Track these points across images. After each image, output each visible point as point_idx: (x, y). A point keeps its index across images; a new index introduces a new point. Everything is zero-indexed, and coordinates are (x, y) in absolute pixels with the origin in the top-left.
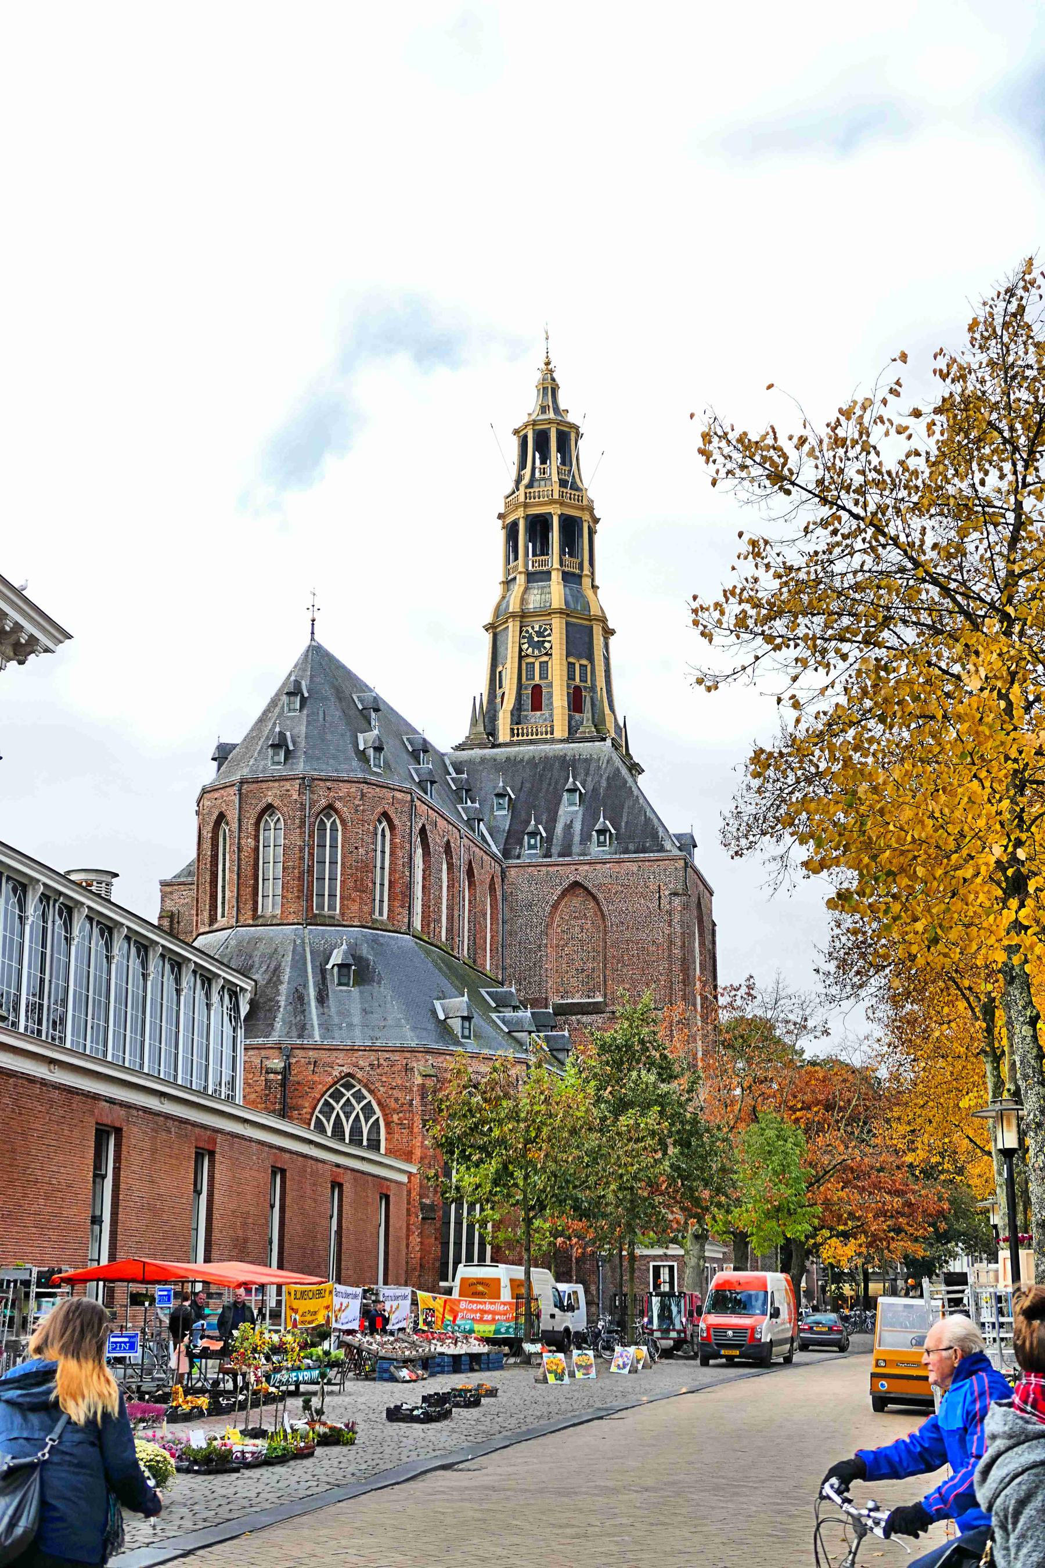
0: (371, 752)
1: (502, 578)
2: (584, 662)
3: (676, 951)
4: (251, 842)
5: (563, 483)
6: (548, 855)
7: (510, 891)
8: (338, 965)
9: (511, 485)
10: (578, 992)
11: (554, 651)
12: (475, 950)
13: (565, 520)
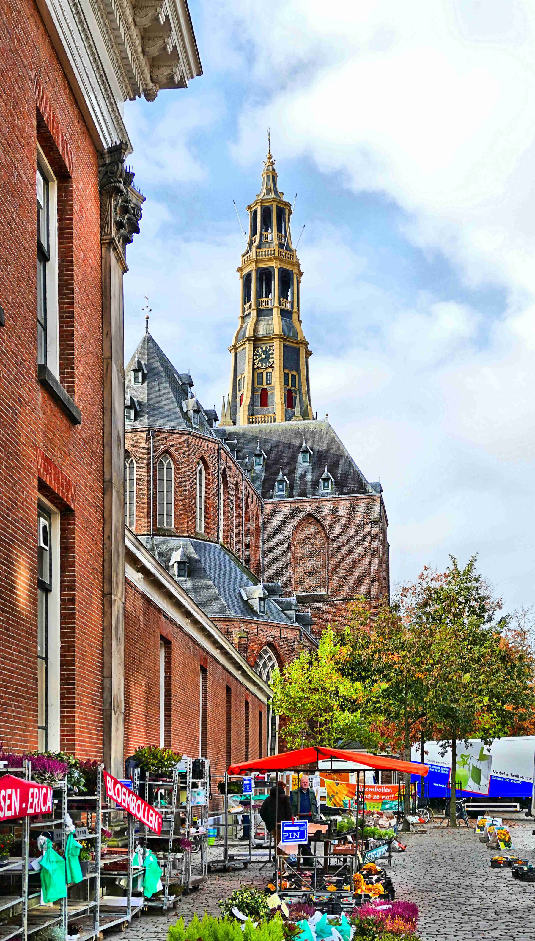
1: (241, 315)
2: (294, 373)
3: (374, 560)
5: (281, 246)
6: (290, 495)
7: (266, 520)
8: (178, 563)
10: (310, 588)
12: (249, 558)
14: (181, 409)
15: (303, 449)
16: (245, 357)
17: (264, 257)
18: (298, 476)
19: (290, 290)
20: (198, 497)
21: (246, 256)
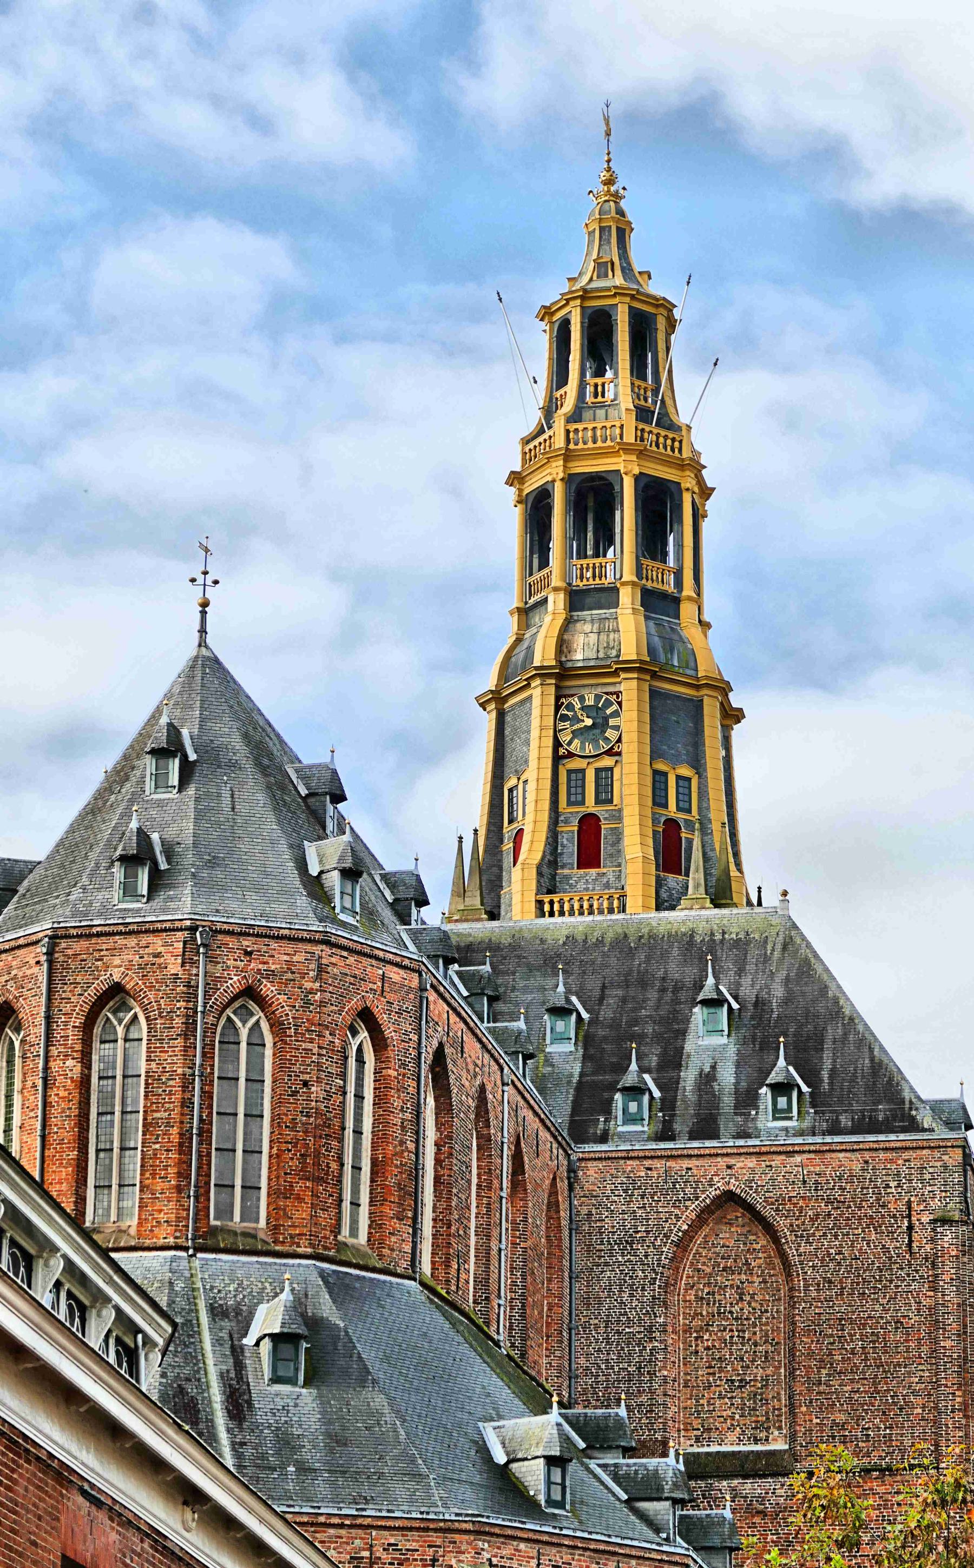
0: (334, 880)
2: (685, 771)
3: (948, 1344)
4: (73, 1067)
5: (643, 414)
6: (666, 1134)
7: (584, 1210)
8: (272, 1336)
9: (535, 417)
10: (732, 1428)
11: (624, 747)
12: (525, 1329)
13: (647, 487)
14: (302, 864)
15: (708, 991)
16: (528, 723)
17: (590, 445)
18: (689, 1078)
19: (671, 539)
20: (349, 1134)
21: (536, 442)
